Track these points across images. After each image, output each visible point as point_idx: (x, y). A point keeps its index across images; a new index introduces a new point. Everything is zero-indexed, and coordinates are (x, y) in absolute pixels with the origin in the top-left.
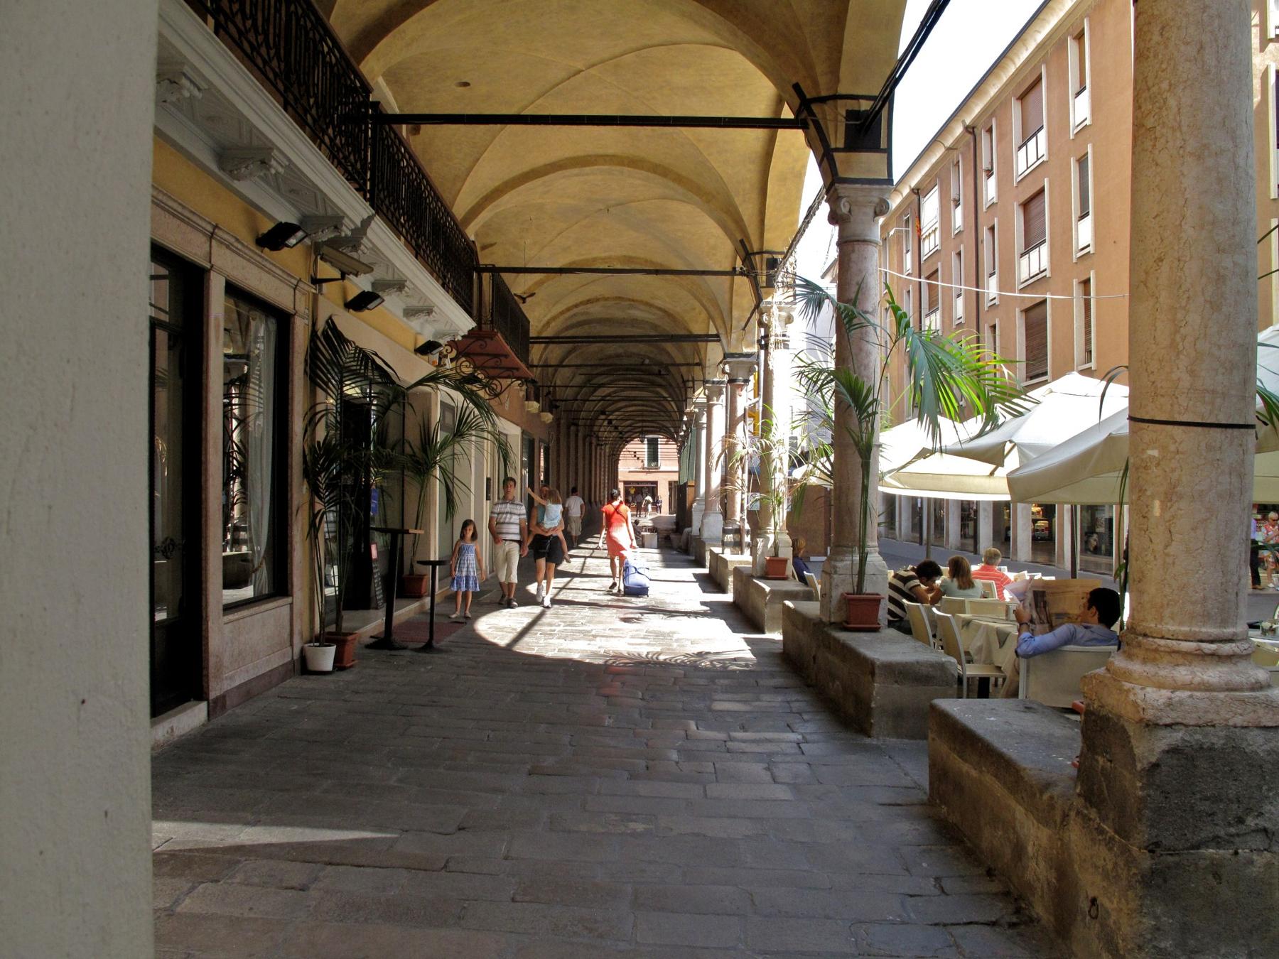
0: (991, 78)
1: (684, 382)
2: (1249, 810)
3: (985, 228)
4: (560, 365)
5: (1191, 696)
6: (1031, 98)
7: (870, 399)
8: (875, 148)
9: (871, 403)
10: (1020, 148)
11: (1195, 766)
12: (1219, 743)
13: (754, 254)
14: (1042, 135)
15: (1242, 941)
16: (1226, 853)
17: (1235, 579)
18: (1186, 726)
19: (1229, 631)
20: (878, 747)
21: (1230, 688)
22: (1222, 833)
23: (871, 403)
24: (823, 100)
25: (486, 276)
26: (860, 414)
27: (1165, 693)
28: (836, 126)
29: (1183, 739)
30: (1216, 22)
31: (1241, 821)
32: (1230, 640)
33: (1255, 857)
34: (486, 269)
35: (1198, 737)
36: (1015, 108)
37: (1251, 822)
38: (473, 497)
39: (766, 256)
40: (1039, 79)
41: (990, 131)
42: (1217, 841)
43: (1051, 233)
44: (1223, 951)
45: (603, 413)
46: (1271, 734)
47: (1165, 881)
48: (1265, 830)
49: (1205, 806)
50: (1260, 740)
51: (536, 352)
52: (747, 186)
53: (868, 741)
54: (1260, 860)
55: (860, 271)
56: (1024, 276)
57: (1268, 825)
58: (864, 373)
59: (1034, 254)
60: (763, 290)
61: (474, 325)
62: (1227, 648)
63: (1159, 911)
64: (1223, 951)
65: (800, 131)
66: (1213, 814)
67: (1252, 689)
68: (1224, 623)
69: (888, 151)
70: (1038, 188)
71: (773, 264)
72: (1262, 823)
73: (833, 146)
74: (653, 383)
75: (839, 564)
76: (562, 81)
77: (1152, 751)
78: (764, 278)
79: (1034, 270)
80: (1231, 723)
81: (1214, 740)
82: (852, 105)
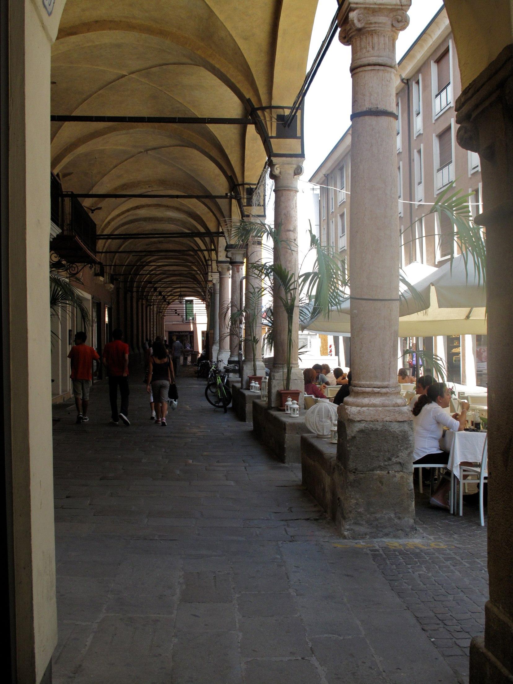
0: (416, 47)
1: (206, 261)
2: (393, 455)
3: (415, 151)
4: (115, 252)
5: (368, 409)
6: (443, 61)
7: (292, 280)
8: (294, 136)
9: (294, 282)
10: (437, 96)
11: (371, 437)
12: (379, 428)
13: (239, 185)
14: (450, 88)
15: (392, 508)
16: (385, 473)
17: (388, 362)
18: (366, 421)
19: (386, 383)
20: (287, 467)
21: (384, 406)
22: (382, 464)
23: (294, 282)
24: (263, 109)
25: (67, 201)
26: (286, 289)
27: (359, 408)
28: (271, 123)
29: (364, 426)
30: (377, 135)
31: (390, 459)
32: (387, 387)
33: (396, 474)
34: (67, 196)
35: (371, 425)
36: (434, 68)
37: (394, 460)
38: (60, 342)
39: (246, 186)
40: (447, 51)
41: (418, 83)
42: (381, 468)
43: (456, 156)
44: (384, 512)
45: (150, 283)
46: (401, 424)
47: (360, 484)
48: (400, 463)
49: (375, 454)
50: (397, 427)
51: (100, 244)
52: (233, 143)
53: (282, 465)
54: (398, 475)
55: (286, 207)
56: (440, 185)
57: (401, 461)
58: (289, 265)
59: (445, 170)
60: (245, 208)
61: (60, 231)
62: (384, 390)
63: (358, 496)
64: (384, 512)
65: (254, 125)
66: (379, 457)
67: (394, 406)
68: (384, 380)
69: (302, 138)
70: (447, 125)
71: (250, 192)
72: (398, 460)
73: (270, 135)
74: (187, 261)
75: (276, 374)
76: (114, 81)
77: (352, 431)
78: (245, 200)
79: (446, 182)
80: (385, 420)
81: (378, 427)
82: (280, 112)
